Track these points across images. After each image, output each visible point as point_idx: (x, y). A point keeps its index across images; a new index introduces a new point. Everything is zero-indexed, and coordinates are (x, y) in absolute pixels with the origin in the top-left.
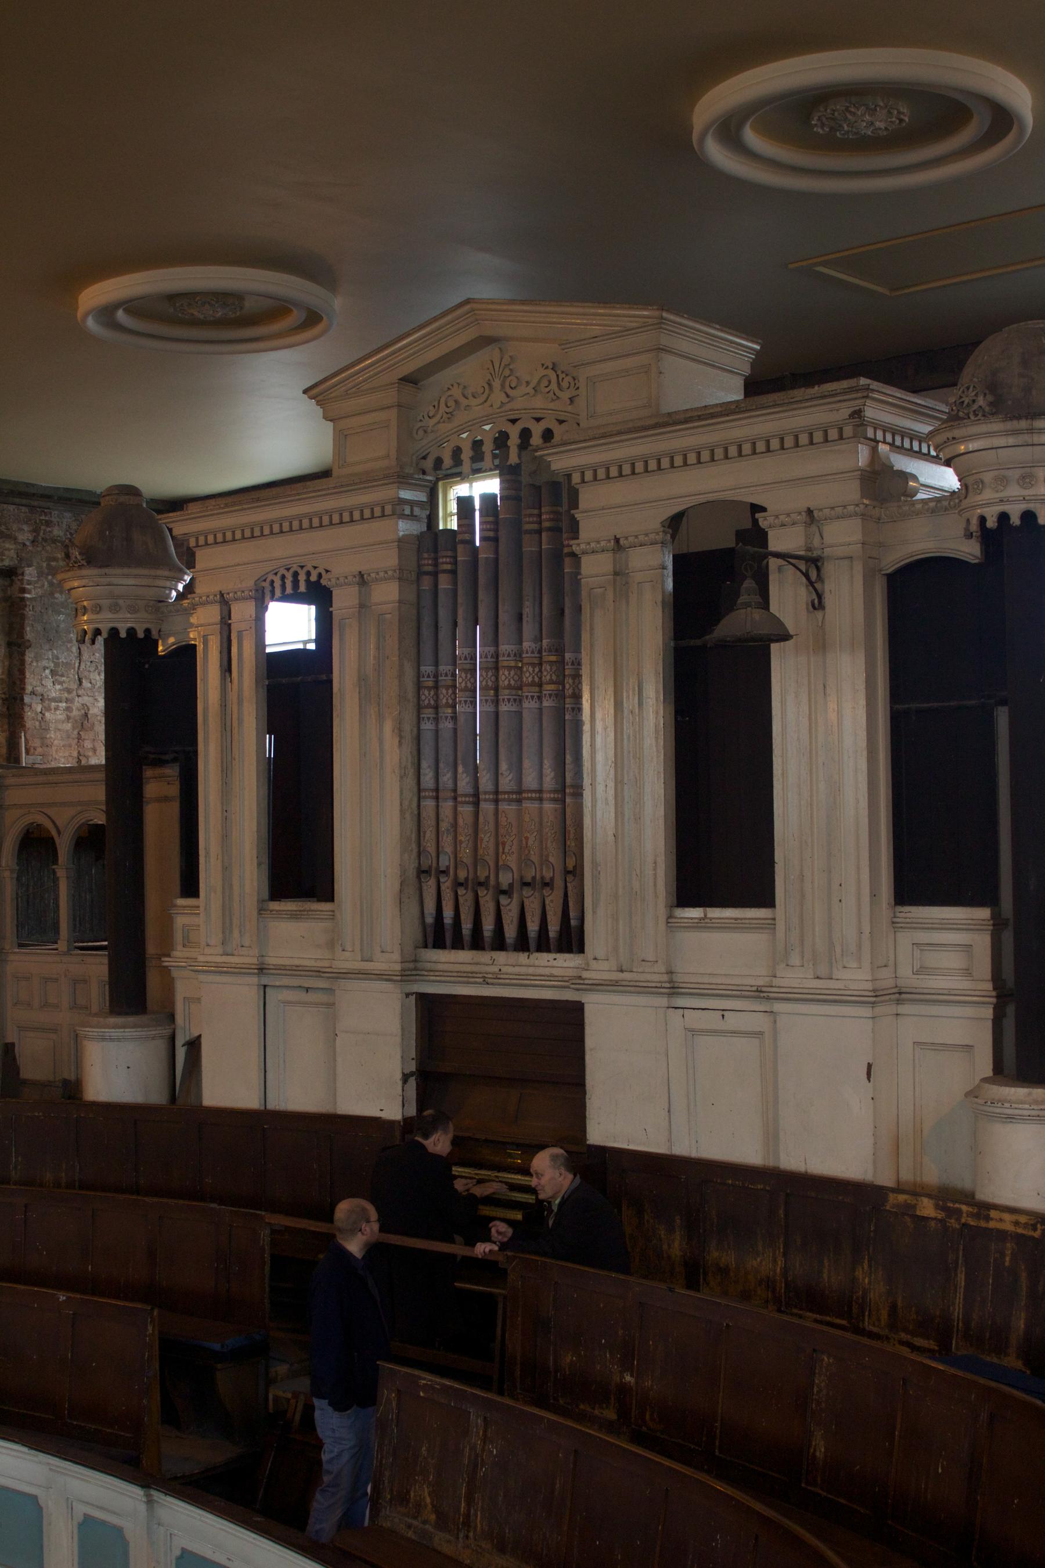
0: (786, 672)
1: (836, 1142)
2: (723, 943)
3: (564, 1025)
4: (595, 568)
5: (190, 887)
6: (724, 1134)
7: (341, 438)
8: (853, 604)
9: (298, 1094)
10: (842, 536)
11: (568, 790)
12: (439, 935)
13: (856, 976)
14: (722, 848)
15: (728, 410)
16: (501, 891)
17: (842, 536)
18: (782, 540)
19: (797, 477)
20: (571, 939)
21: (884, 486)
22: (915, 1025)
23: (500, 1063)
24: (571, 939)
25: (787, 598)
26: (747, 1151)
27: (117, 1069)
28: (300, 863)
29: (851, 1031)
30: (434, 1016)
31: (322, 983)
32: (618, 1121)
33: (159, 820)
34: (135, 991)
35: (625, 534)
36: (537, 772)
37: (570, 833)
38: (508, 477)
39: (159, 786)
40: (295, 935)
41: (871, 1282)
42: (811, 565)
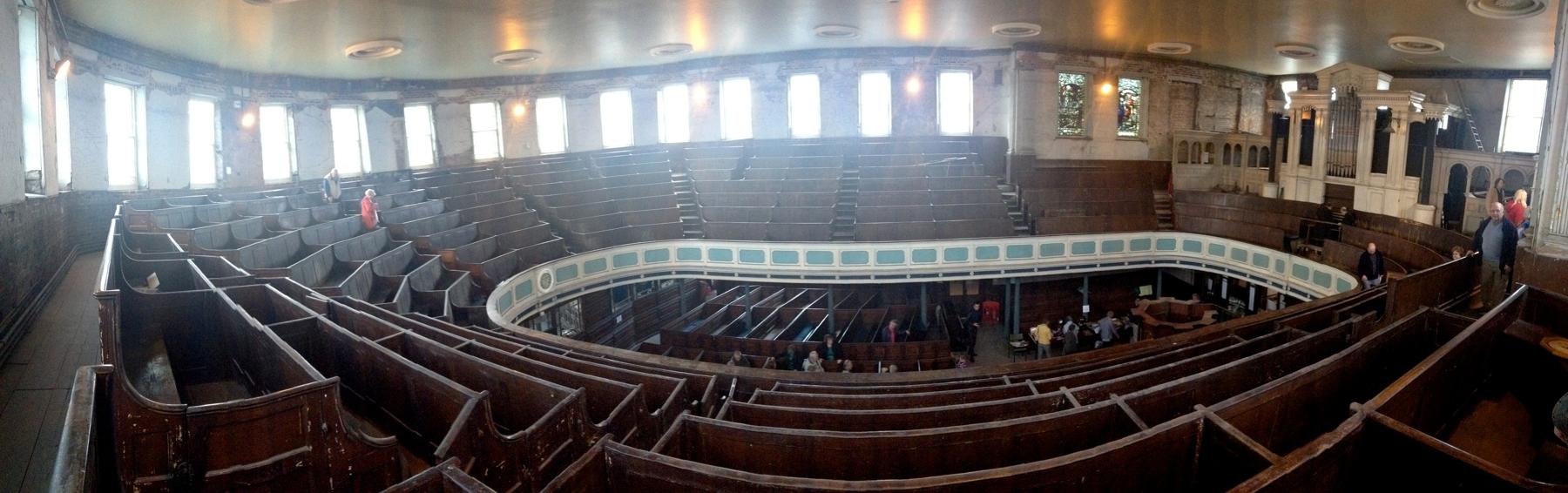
0: (1393, 136)
1: (1393, 211)
2: (1378, 179)
3: (1351, 190)
4: (1363, 114)
5: (1285, 160)
6: (1375, 209)
7: (857, 75)
8: (1404, 127)
9: (1302, 199)
10: (1404, 116)
11: (1355, 152)
12: (1330, 174)
13: (1398, 186)
14: (1379, 164)
15: (1550, 87)
16: (1341, 167)
17: (1404, 116)
18: (1394, 115)
19: (1398, 107)
20: (1353, 176)
21: (1412, 108)
22: (1407, 194)
23: (1340, 196)
24: (1353, 176)
25: (1394, 125)
26: (1377, 211)
27: (1269, 192)
28: (1306, 158)
29: (1397, 194)
30: (1328, 186)
31: (1308, 181)
32: (1358, 206)
33: (1280, 148)
34: (1272, 178)
35: (1371, 108)
36: (1350, 148)
37: (1354, 159)
38: (336, 191)
39: (1280, 141)
40: (1304, 171)
41: (1396, 232)
42: (1399, 120)
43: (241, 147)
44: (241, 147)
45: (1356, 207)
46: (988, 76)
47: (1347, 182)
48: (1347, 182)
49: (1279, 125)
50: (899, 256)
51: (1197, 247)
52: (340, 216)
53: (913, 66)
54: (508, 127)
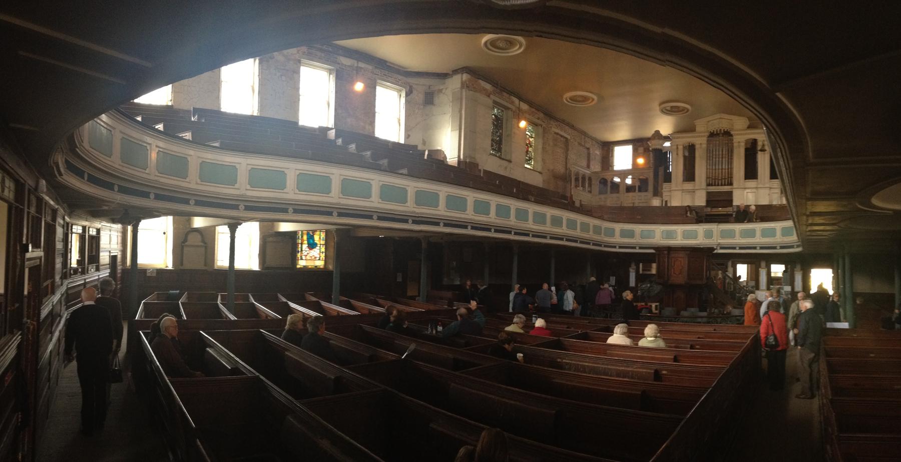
3: (730, 194)
4: (735, 145)
12: (708, 185)
22: (773, 191)
24: (731, 184)
27: (656, 202)
28: (689, 176)
29: (767, 191)
30: (709, 194)
31: (693, 192)
35: (740, 140)
36: (725, 166)
43: (280, 87)
44: (280, 87)
45: (704, 204)
46: (419, 97)
47: (726, 188)
48: (726, 188)
49: (659, 158)
50: (611, 233)
51: (752, 233)
52: (540, 196)
53: (358, 70)
54: (342, 97)
